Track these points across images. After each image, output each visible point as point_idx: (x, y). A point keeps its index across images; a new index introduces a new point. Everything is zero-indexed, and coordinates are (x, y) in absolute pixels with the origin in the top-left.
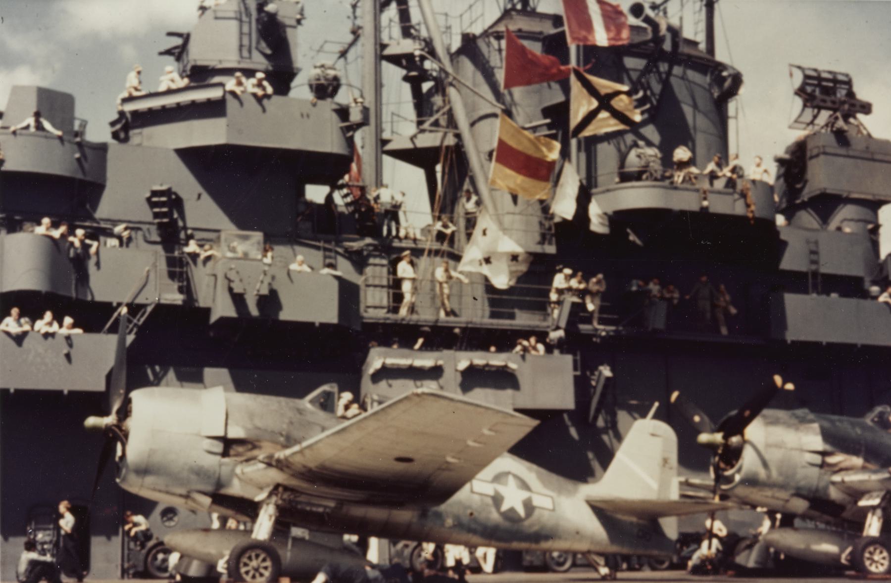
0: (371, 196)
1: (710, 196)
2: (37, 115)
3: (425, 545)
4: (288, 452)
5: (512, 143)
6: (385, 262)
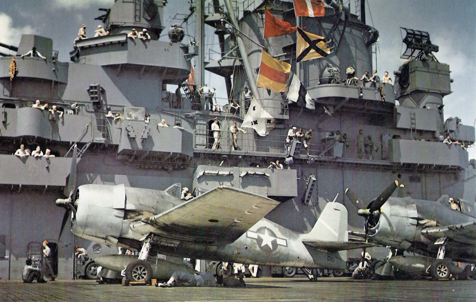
0: (199, 90)
1: (363, 91)
2: (34, 50)
3: (223, 263)
4: (156, 217)
5: (267, 64)
6: (205, 123)
